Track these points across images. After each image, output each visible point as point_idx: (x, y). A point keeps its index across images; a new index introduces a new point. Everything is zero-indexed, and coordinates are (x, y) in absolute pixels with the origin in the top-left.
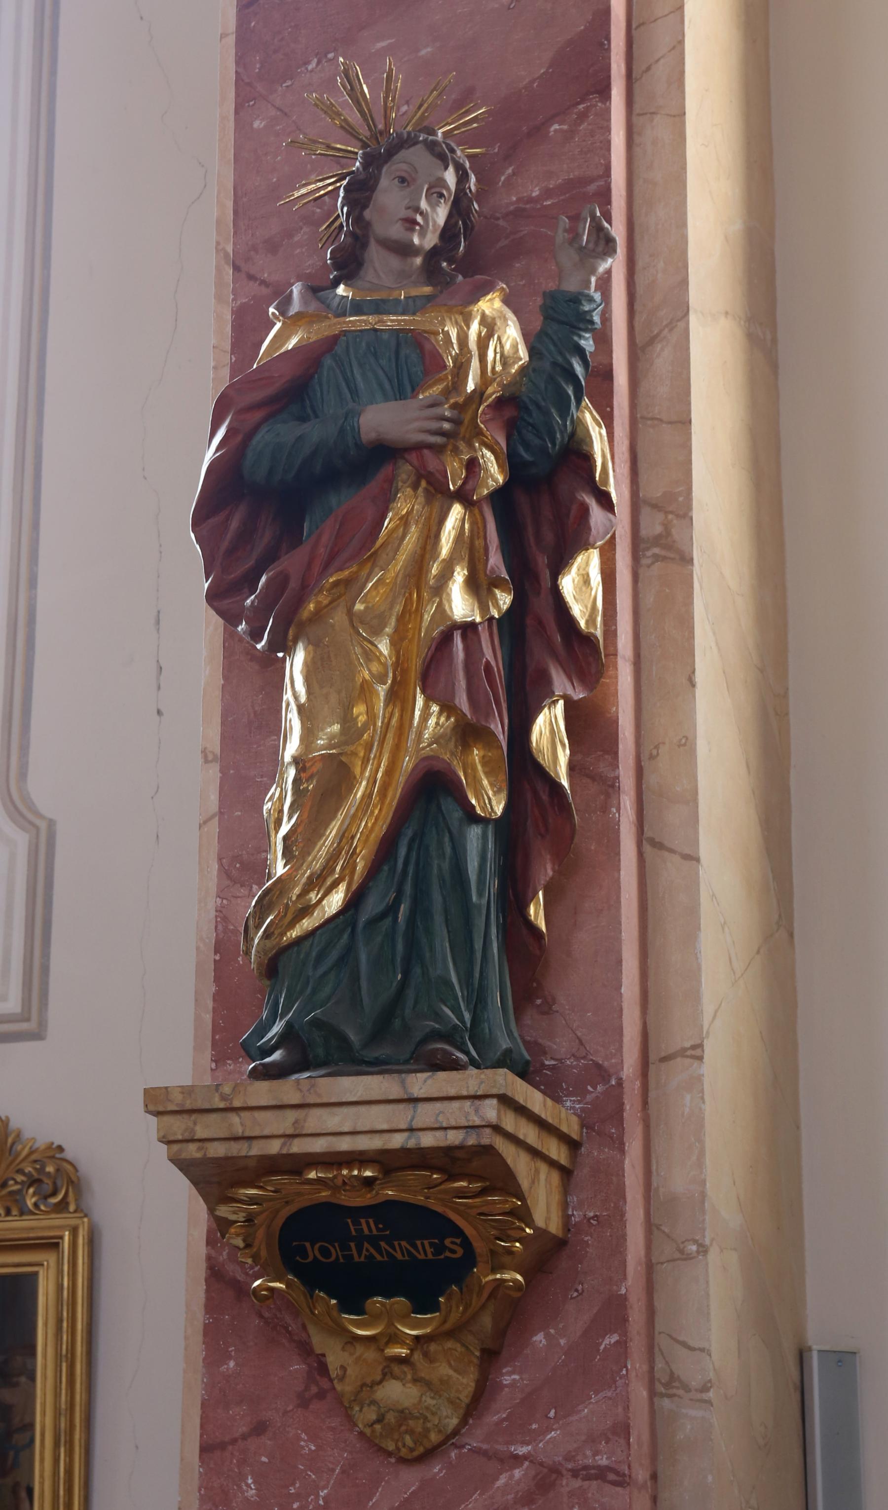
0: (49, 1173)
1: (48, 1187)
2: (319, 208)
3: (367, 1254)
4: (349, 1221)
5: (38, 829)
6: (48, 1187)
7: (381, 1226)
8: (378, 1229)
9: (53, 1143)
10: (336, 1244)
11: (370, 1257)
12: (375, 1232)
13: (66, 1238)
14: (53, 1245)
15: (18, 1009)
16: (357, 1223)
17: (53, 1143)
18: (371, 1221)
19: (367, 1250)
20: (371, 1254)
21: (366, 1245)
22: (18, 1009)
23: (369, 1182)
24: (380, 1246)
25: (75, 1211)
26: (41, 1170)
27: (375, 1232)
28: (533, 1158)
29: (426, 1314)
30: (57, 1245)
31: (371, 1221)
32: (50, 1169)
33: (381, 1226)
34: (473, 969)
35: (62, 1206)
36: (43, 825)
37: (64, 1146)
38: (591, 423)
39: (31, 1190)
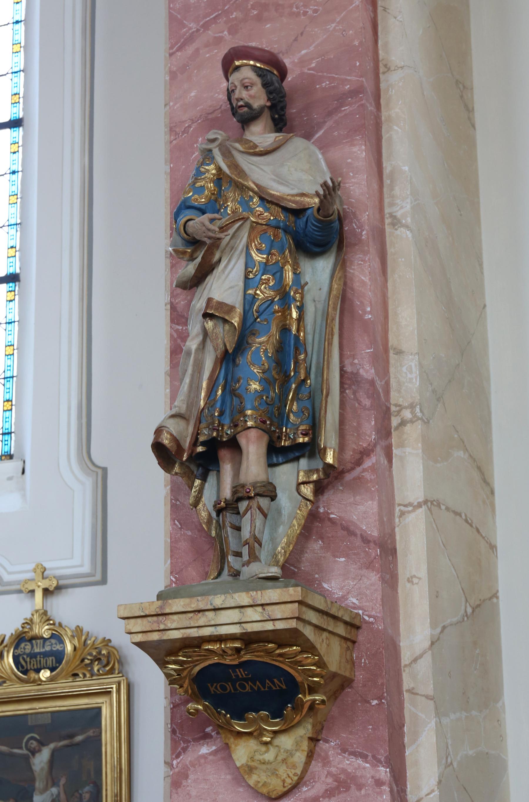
0: (104, 654)
1: (104, 661)
2: (257, 294)
6: (104, 661)
7: (246, 673)
8: (246, 675)
9: (105, 638)
10: (229, 683)
11: (270, 688)
12: (244, 676)
13: (115, 689)
14: (108, 693)
16: (234, 671)
17: (105, 638)
18: (241, 670)
19: (268, 684)
20: (270, 686)
22: (86, 569)
23: (238, 650)
24: (274, 681)
25: (119, 673)
26: (100, 653)
27: (244, 676)
29: (241, 721)
31: (241, 670)
32: (104, 652)
33: (246, 673)
35: (111, 671)
37: (112, 640)
38: (224, 261)
39: (97, 663)
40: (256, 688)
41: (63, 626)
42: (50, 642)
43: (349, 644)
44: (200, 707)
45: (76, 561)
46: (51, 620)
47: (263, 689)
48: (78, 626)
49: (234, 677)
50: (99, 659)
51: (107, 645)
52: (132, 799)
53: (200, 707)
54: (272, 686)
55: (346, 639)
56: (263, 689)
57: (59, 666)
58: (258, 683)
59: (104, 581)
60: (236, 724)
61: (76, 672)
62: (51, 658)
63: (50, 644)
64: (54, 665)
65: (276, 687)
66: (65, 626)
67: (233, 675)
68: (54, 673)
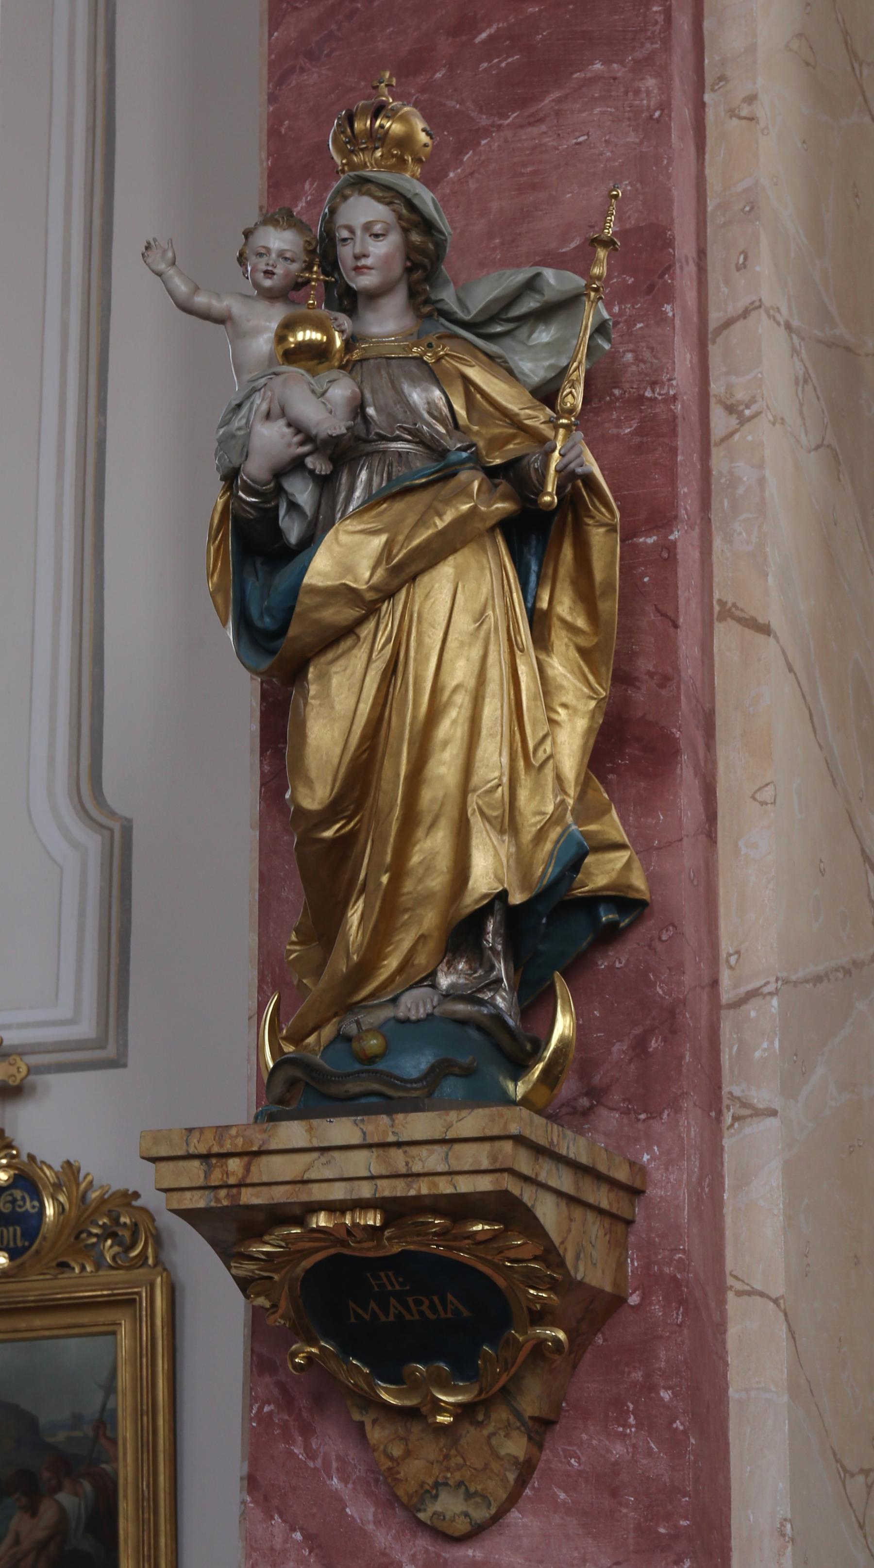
3: (397, 1312)
4: (369, 1275)
5: (112, 831)
7: (401, 1280)
8: (400, 1284)
10: (353, 1320)
12: (397, 1287)
14: (130, 1302)
15: (86, 1029)
21: (393, 1301)
22: (86, 1029)
26: (116, 1221)
28: (537, 1160)
30: (114, 1333)
31: (391, 1274)
33: (401, 1280)
34: (417, 636)
36: (117, 827)
37: (140, 1192)
40: (367, 1317)
41: (38, 1160)
42: (11, 1195)
43: (620, 1227)
44: (313, 1350)
45: (65, 1011)
46: (13, 1148)
47: (383, 1318)
48: (68, 1163)
49: (376, 1289)
50: (113, 1235)
51: (129, 1205)
52: (179, 1513)
53: (313, 1350)
54: (405, 1313)
55: (614, 1217)
56: (383, 1318)
57: (31, 1244)
58: (373, 1305)
59: (117, 1063)
60: (383, 1388)
61: (65, 1259)
62: (11, 1229)
63: (10, 1198)
64: (19, 1244)
65: (412, 1315)
66: (43, 1162)
67: (373, 1283)
68: (18, 1262)
